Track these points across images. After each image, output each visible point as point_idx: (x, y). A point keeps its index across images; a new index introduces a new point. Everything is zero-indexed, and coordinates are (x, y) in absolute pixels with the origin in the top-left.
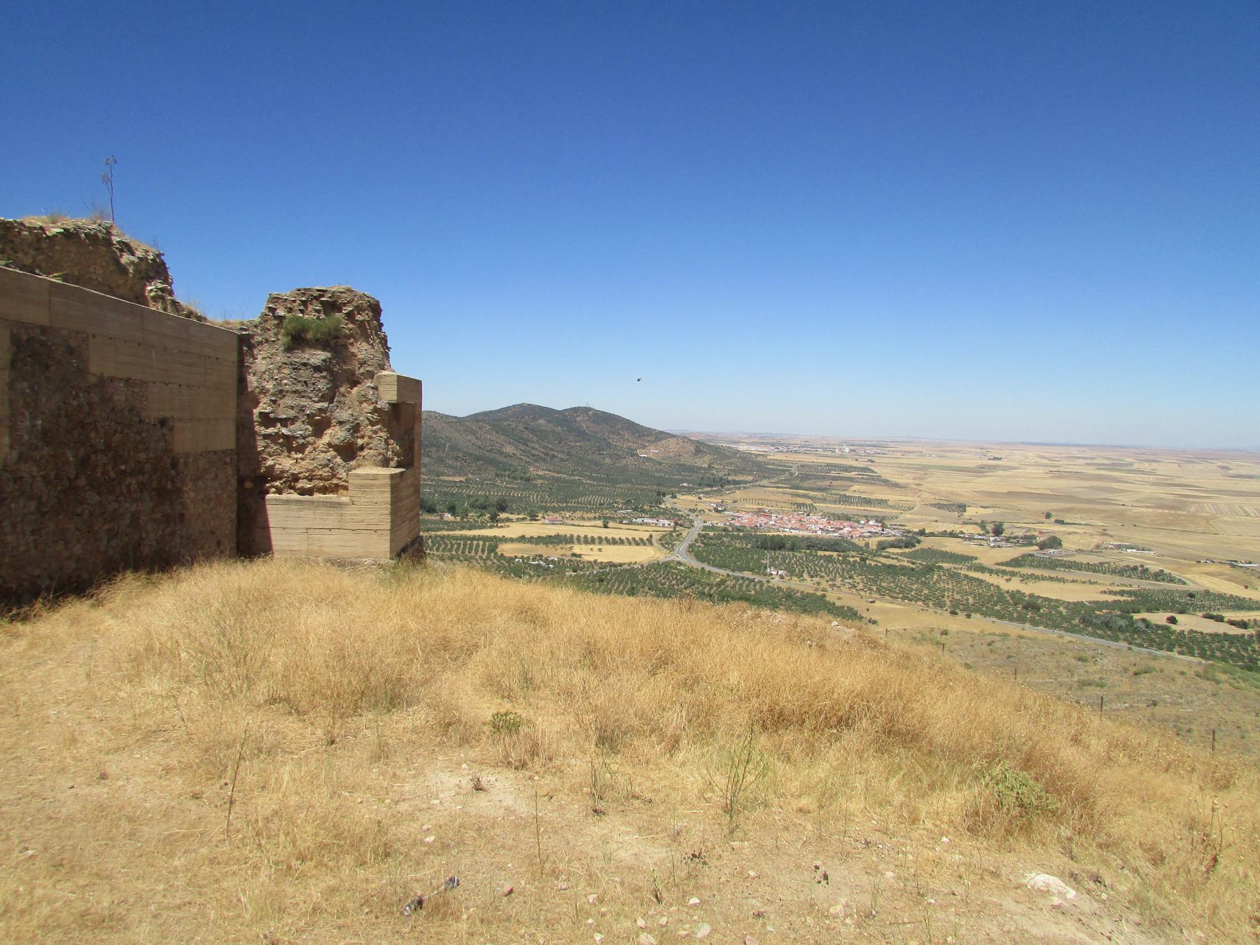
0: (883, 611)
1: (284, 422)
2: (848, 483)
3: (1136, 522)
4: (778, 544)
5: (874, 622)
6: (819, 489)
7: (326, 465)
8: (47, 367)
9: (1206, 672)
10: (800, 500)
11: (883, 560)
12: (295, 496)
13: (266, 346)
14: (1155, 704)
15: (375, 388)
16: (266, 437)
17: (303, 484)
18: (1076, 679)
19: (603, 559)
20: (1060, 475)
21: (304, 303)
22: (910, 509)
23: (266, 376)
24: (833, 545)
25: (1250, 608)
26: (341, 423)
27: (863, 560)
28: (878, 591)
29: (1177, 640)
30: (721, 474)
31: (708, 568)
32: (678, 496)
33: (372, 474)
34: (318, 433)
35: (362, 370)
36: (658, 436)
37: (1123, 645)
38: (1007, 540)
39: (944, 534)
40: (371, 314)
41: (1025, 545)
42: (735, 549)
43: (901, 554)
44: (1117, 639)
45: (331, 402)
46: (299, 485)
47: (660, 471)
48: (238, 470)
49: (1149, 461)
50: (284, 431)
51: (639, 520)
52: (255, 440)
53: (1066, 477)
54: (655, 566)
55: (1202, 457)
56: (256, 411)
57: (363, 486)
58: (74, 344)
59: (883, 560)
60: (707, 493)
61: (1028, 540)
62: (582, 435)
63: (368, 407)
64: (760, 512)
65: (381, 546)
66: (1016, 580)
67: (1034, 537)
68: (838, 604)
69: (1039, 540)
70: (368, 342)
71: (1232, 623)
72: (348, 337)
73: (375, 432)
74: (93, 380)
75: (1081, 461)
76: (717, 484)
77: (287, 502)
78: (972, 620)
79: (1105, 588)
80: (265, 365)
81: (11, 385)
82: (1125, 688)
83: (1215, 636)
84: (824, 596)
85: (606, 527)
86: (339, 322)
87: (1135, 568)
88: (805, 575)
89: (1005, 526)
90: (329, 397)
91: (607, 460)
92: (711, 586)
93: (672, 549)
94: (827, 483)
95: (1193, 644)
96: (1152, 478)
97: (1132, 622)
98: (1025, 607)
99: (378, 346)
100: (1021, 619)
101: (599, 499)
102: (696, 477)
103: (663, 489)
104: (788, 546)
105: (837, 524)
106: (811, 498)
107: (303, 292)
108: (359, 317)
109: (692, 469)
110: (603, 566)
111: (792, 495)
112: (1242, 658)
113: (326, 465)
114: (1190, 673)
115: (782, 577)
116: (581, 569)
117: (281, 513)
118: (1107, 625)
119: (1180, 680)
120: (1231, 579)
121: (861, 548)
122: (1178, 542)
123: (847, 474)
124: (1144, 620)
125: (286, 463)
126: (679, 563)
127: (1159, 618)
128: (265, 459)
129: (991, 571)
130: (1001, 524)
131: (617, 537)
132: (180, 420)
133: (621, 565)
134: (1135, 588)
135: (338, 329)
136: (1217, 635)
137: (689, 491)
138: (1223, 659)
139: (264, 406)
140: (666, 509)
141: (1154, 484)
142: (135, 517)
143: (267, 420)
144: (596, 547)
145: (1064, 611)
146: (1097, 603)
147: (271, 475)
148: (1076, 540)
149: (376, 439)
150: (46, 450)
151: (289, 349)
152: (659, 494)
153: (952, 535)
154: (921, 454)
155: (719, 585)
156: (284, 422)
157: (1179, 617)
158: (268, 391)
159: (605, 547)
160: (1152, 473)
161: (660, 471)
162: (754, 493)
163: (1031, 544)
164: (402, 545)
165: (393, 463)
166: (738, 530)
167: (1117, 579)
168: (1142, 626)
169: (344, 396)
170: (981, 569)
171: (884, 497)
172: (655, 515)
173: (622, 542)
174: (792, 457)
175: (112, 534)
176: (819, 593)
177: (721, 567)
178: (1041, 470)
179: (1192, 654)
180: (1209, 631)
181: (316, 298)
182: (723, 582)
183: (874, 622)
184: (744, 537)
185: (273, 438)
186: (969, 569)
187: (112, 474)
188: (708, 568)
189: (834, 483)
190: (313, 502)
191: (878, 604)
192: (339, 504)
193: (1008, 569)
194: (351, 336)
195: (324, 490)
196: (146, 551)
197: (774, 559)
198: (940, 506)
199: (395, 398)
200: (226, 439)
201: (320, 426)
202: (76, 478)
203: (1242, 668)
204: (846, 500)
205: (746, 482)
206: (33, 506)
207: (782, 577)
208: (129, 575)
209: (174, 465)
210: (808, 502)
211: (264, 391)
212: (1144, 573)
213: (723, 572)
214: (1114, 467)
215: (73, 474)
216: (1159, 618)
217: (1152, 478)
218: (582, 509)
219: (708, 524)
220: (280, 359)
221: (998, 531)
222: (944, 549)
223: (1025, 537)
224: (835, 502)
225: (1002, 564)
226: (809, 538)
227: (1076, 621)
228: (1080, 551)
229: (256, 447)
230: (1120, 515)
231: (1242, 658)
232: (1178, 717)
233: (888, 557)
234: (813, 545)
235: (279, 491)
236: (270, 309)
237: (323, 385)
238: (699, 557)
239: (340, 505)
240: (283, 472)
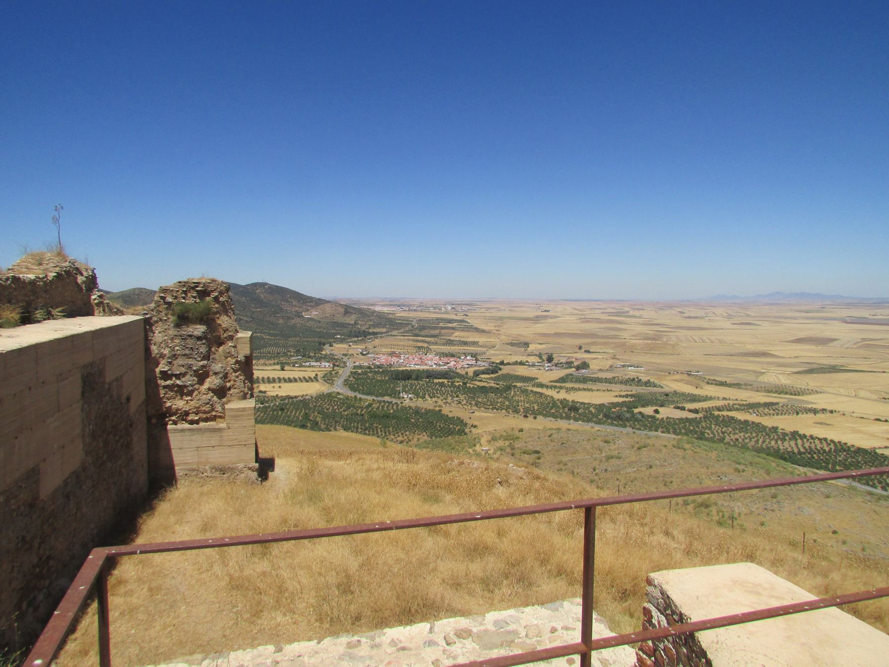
0: (480, 418)
1: (178, 377)
2: (452, 331)
3: (632, 349)
4: (407, 376)
5: (475, 427)
6: (432, 336)
7: (208, 403)
9: (678, 443)
10: (420, 344)
11: (478, 383)
12: (187, 426)
14: (651, 467)
16: (165, 387)
17: (191, 417)
18: (604, 455)
19: (282, 393)
20: (586, 321)
21: (185, 292)
22: (493, 347)
23: (163, 345)
24: (445, 375)
25: (699, 401)
26: (216, 374)
27: (465, 384)
28: (476, 405)
29: (660, 424)
30: (363, 328)
31: (359, 396)
32: (334, 345)
34: (201, 382)
35: (225, 335)
36: (318, 302)
37: (629, 429)
38: (556, 365)
39: (516, 363)
41: (567, 368)
42: (377, 381)
43: (489, 379)
44: (625, 426)
45: (209, 360)
46: (190, 418)
47: (320, 328)
48: (147, 412)
49: (638, 309)
50: (178, 382)
51: (308, 364)
52: (158, 391)
53: (590, 322)
54: (321, 397)
55: (670, 306)
56: (158, 370)
57: (235, 416)
59: (478, 383)
60: (355, 342)
61: (569, 364)
62: (260, 302)
64: (392, 354)
66: (563, 391)
67: (572, 362)
68: (450, 415)
69: (575, 364)
71: (690, 411)
72: (216, 313)
73: (237, 377)
75: (598, 311)
76: (363, 335)
77: (183, 430)
78: (537, 420)
79: (617, 394)
80: (162, 337)
82: (633, 458)
83: (681, 420)
84: (440, 411)
85: (283, 370)
87: (634, 379)
88: (427, 397)
89: (554, 356)
91: (281, 321)
92: (362, 408)
93: (332, 384)
94: (438, 331)
95: (669, 426)
96: (640, 320)
97: (633, 415)
98: (570, 409)
100: (568, 418)
101: (276, 350)
102: (345, 330)
103: (323, 341)
104: (414, 376)
105: (445, 360)
106: (428, 342)
108: (221, 299)
109: (343, 325)
110: (283, 398)
111: (414, 340)
112: (696, 432)
113: (208, 403)
114: (670, 445)
115: (411, 399)
116: (267, 402)
118: (619, 417)
119: (664, 450)
120: (687, 383)
121: (463, 376)
122: (658, 361)
123: (450, 325)
124: (640, 413)
125: (179, 404)
126: (338, 393)
127: (649, 411)
128: (165, 402)
129: (547, 387)
130: (552, 354)
131: (292, 377)
133: (296, 397)
134: (634, 392)
135: (210, 309)
136: (682, 419)
137: (342, 341)
138: (686, 434)
139: (162, 367)
140: (326, 355)
141: (644, 324)
143: (165, 375)
144: (277, 385)
145: (593, 410)
146: (612, 403)
147: (170, 412)
148: (598, 363)
152: (320, 343)
153: (522, 363)
154: (499, 310)
155: (367, 407)
156: (178, 377)
157: (660, 409)
158: (165, 355)
159: (283, 385)
160: (639, 317)
161: (320, 328)
162: (387, 341)
163: (571, 367)
166: (378, 367)
167: (623, 387)
168: (640, 417)
170: (541, 385)
171: (476, 340)
172: (318, 360)
173: (295, 380)
174: (412, 315)
176: (437, 409)
177: (368, 394)
178: (574, 318)
179: (669, 432)
180: (678, 417)
181: (193, 288)
182: (370, 405)
183: (475, 427)
184: (383, 372)
186: (533, 386)
188: (359, 396)
189: (443, 331)
191: (477, 413)
193: (558, 384)
194: (217, 312)
195: (206, 420)
197: (405, 387)
198: (512, 344)
199: (249, 352)
201: (202, 376)
203: (697, 439)
204: (450, 343)
205: (382, 333)
207: (411, 399)
210: (425, 345)
211: (162, 356)
212: (638, 382)
213: (370, 398)
214: (618, 314)
216: (649, 411)
217: (640, 320)
218: (264, 357)
219: (357, 364)
220: (172, 332)
221: (550, 359)
222: (517, 374)
223: (567, 363)
224: (443, 345)
225: (556, 381)
226: (428, 370)
227: (601, 417)
228: (600, 370)
229: (159, 394)
230: (623, 345)
231: (696, 432)
232: (665, 475)
233: (481, 381)
234: (431, 375)
235: (175, 423)
237: (203, 350)
238: (352, 388)
239: (220, 430)
240: (178, 410)
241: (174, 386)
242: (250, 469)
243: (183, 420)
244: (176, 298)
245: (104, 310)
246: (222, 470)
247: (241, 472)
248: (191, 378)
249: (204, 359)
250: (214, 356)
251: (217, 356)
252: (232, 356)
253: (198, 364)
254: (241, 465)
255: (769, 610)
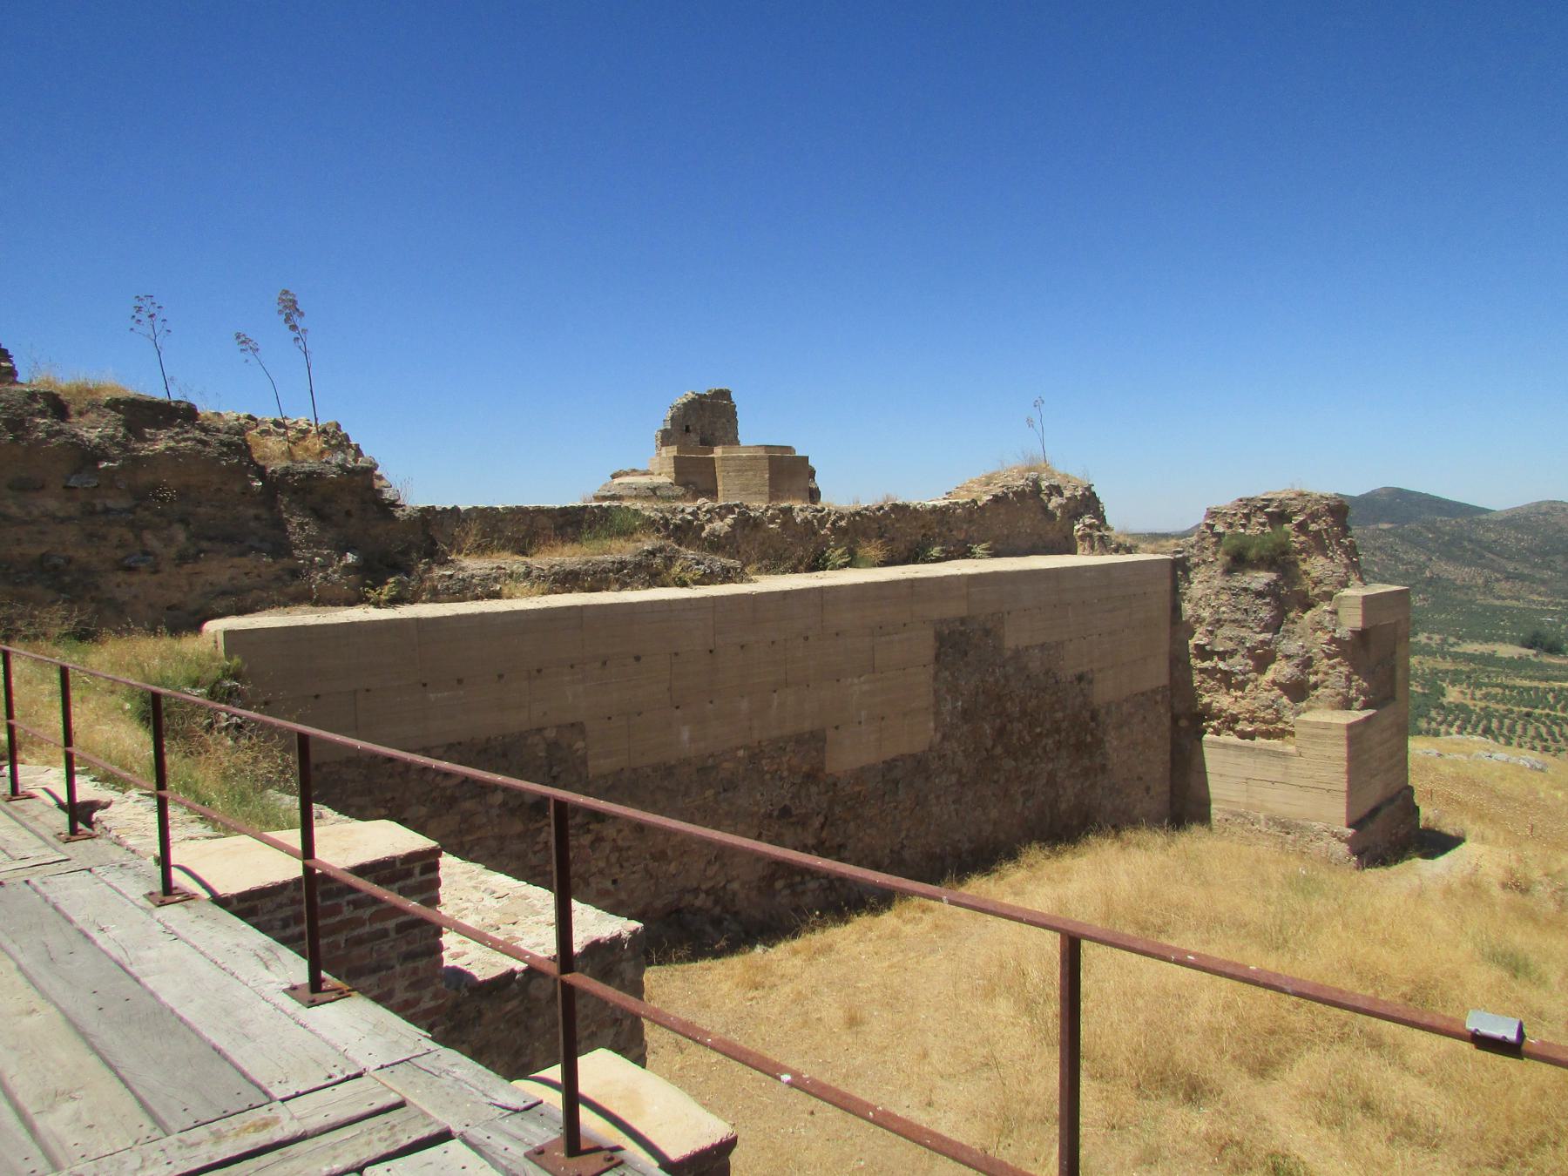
1: (1222, 656)
8: (966, 654)
12: (1234, 739)
13: (1203, 568)
15: (1334, 612)
16: (1202, 671)
21: (1247, 516)
23: (1202, 603)
26: (1288, 657)
33: (1328, 720)
35: (1316, 591)
40: (1330, 519)
46: (1238, 727)
48: (1172, 707)
50: (1221, 665)
56: (1191, 642)
57: (1313, 736)
58: (989, 625)
63: (1323, 637)
65: (1331, 812)
70: (1326, 556)
73: (1333, 667)
74: (1008, 654)
77: (1225, 746)
80: (1204, 591)
81: (936, 678)
86: (1288, 534)
90: (1274, 626)
99: (1341, 558)
107: (1245, 502)
108: (1313, 527)
117: (1226, 767)
125: (1223, 701)
132: (1100, 670)
139: (1199, 638)
142: (1052, 776)
143: (1203, 653)
147: (1207, 713)
149: (1333, 676)
150: (965, 727)
151: (1228, 572)
164: (1370, 803)
165: (1356, 704)
169: (1293, 622)
175: (1028, 795)
181: (1261, 509)
185: (1210, 673)
187: (1028, 739)
190: (1253, 749)
192: (1285, 754)
195: (1268, 735)
196: (1063, 806)
200: (1156, 675)
201: (1263, 660)
202: (994, 747)
206: (954, 778)
208: (1035, 845)
209: (1094, 717)
211: (1200, 620)
215: (989, 744)
220: (1218, 582)
229: (1192, 682)
235: (1217, 732)
236: (1208, 526)
237: (1265, 613)
239: (1285, 755)
240: (1221, 710)
241: (1215, 670)
242: (1335, 835)
243: (1230, 729)
244: (1231, 525)
245: (1092, 547)
246: (1286, 827)
247: (1318, 837)
248: (1243, 661)
249: (1265, 629)
250: (1291, 626)
251: (1297, 629)
252: (1323, 629)
253: (1255, 637)
254: (1319, 826)
255: (845, 1096)
